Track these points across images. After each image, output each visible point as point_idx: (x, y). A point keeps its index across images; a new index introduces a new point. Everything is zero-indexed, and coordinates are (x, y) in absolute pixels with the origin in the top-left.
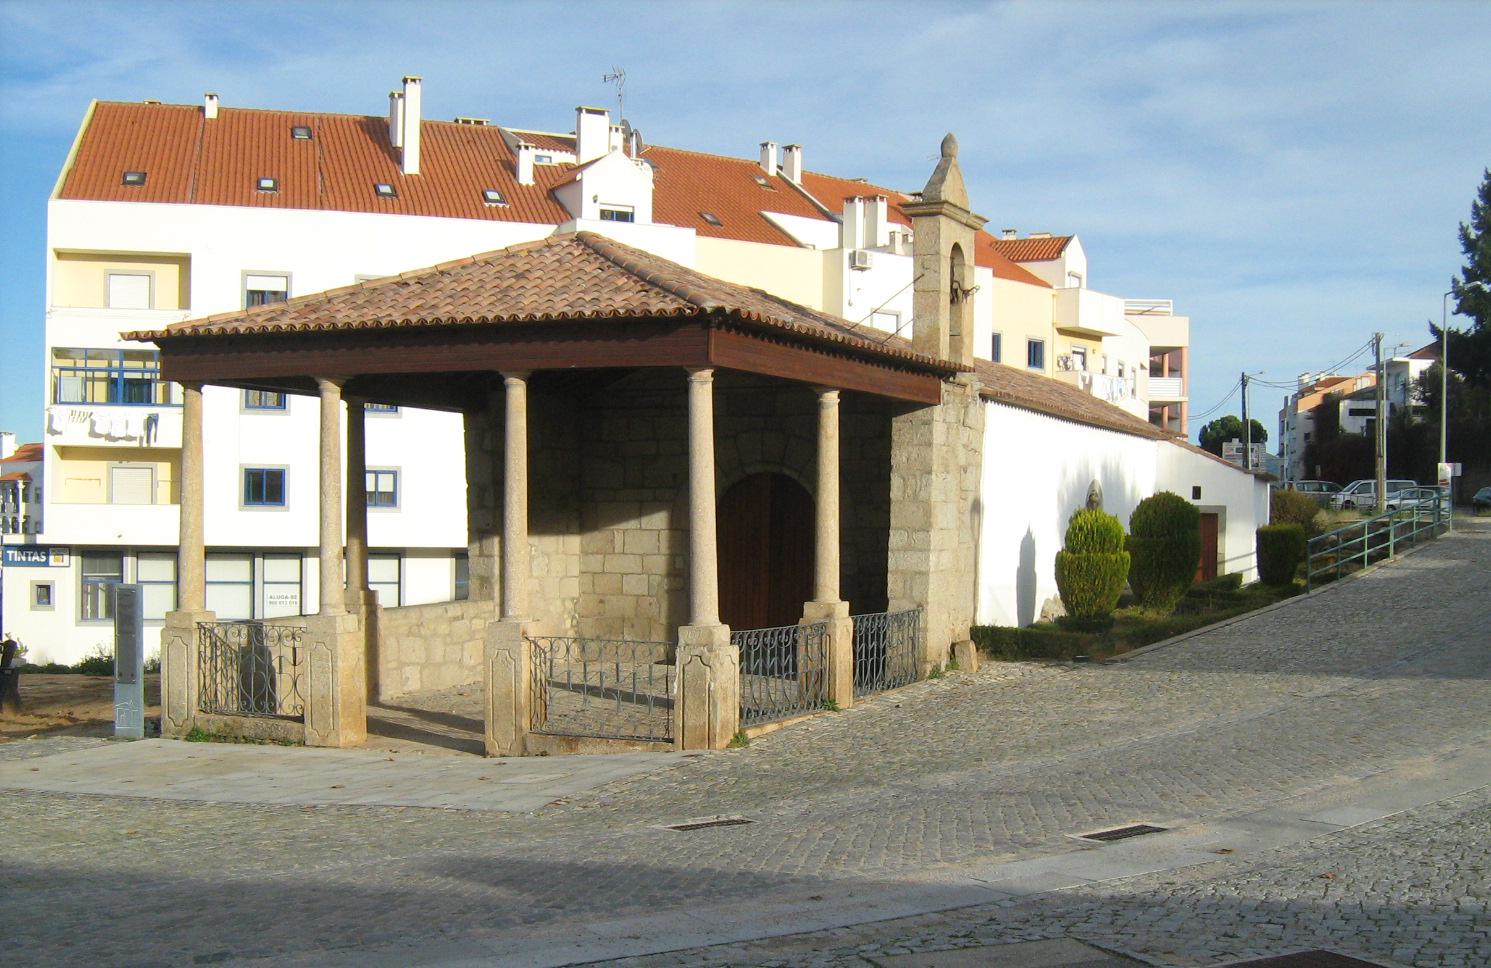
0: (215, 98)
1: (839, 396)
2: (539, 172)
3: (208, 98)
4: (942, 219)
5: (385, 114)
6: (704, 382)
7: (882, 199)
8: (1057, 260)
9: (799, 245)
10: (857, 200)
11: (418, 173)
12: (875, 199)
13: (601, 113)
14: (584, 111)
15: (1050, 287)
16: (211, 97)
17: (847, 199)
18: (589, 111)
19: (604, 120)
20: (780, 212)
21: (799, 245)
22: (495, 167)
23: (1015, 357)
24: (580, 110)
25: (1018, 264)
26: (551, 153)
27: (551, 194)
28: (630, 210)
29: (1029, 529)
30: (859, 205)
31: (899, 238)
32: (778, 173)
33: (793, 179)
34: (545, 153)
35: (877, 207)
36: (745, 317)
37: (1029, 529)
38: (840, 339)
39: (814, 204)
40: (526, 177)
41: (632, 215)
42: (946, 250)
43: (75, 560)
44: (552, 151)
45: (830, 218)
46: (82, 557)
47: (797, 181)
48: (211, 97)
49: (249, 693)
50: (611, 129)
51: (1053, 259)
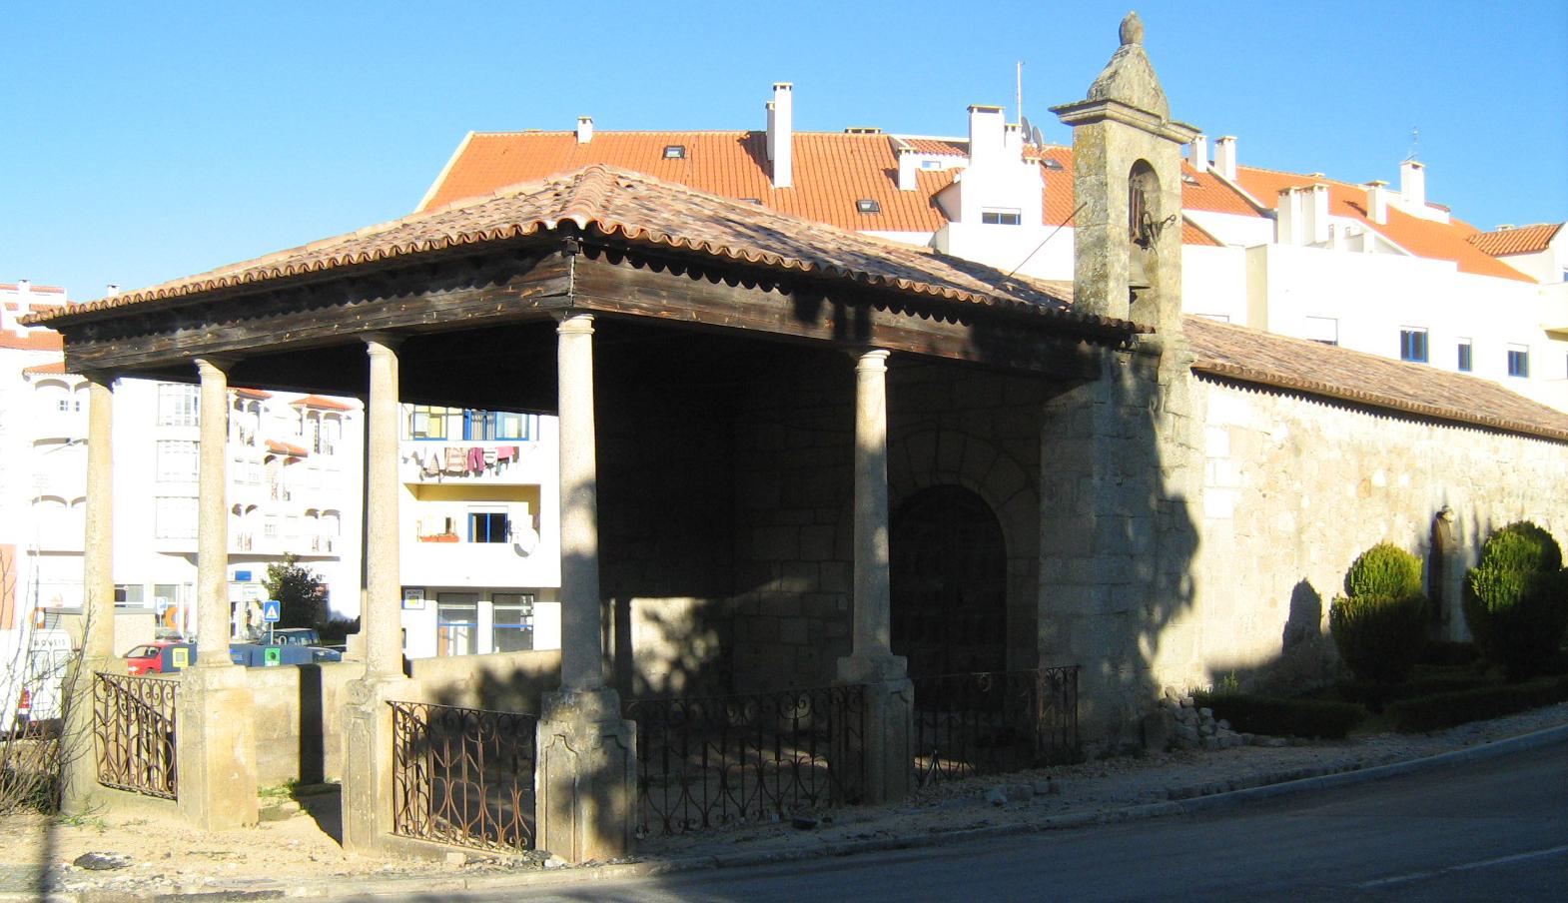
0: (588, 121)
1: (887, 362)
2: (920, 177)
3: (581, 122)
4: (1106, 123)
5: (763, 128)
6: (574, 333)
7: (1320, 188)
8: (1545, 251)
9: (1218, 244)
10: (1292, 192)
11: (790, 186)
12: (1312, 189)
13: (996, 111)
14: (975, 110)
15: (1536, 282)
16: (584, 121)
17: (1281, 192)
18: (980, 110)
19: (999, 119)
20: (1201, 208)
21: (1218, 244)
22: (876, 176)
23: (1490, 367)
24: (971, 109)
25: (1498, 259)
26: (940, 157)
27: (935, 201)
28: (1017, 212)
29: (539, 533)
30: (1295, 197)
31: (1340, 234)
32: (1208, 170)
33: (1225, 174)
34: (934, 157)
35: (1314, 198)
36: (1081, 320)
37: (539, 533)
38: (734, 253)
39: (1247, 201)
40: (907, 181)
41: (1019, 216)
42: (1118, 169)
43: (432, 606)
44: (941, 156)
45: (1264, 213)
46: (493, 602)
47: (1230, 176)
48: (584, 121)
49: (476, 759)
50: (1006, 128)
51: (1540, 250)
